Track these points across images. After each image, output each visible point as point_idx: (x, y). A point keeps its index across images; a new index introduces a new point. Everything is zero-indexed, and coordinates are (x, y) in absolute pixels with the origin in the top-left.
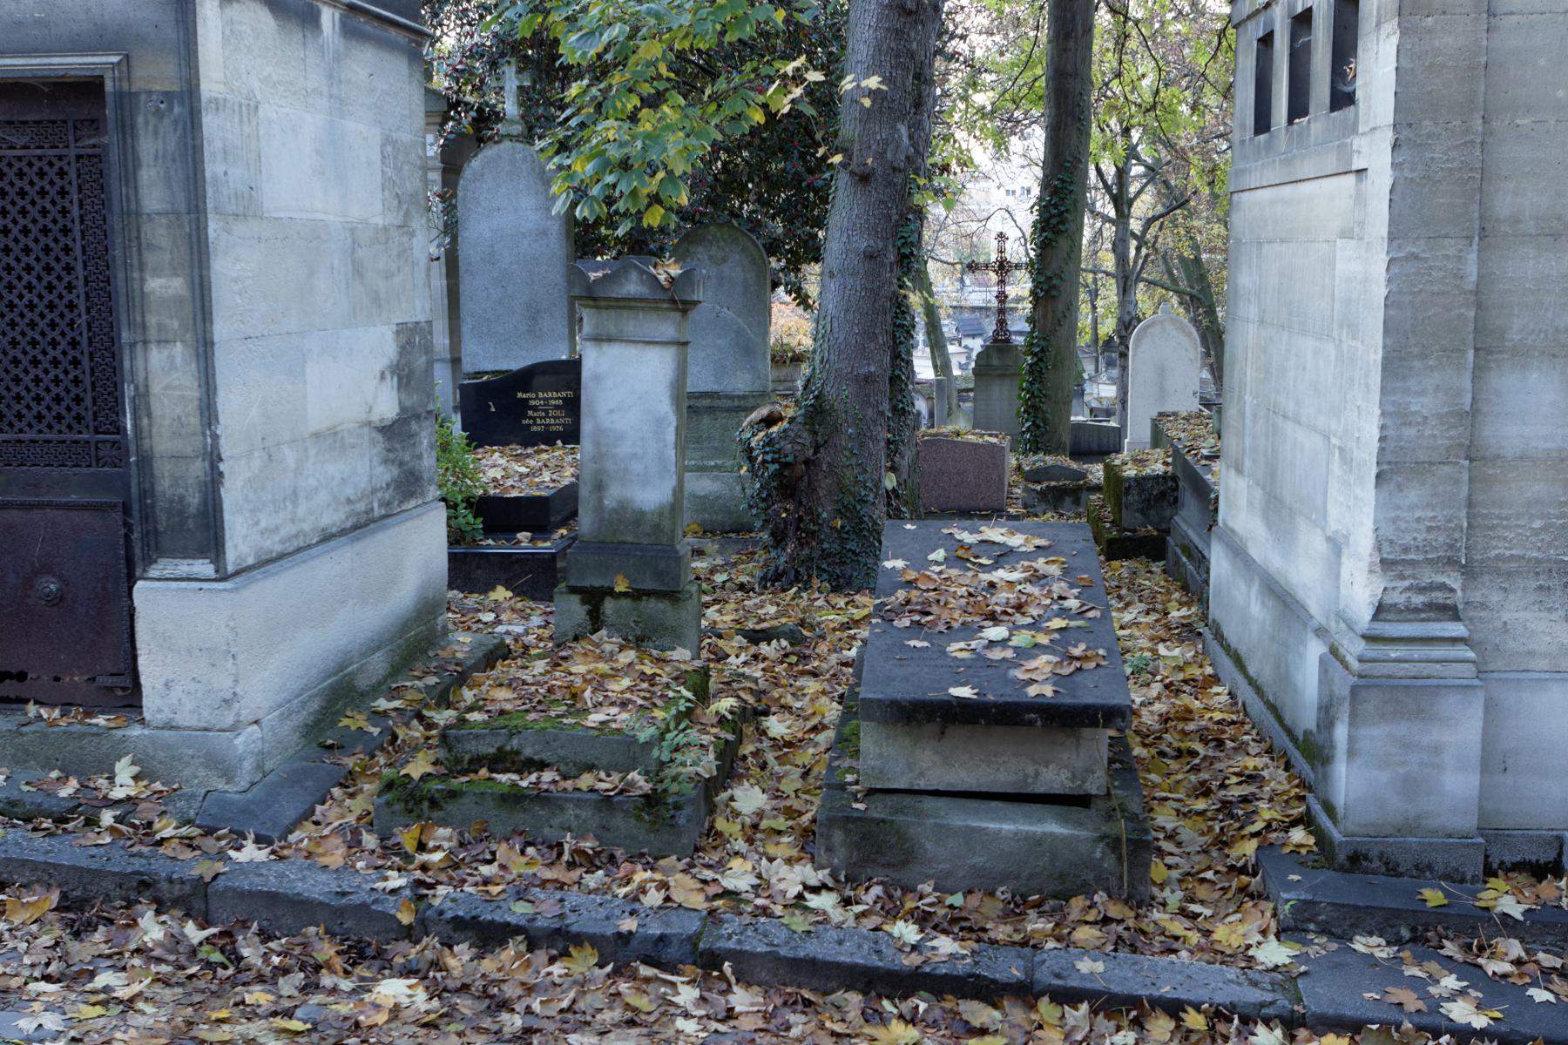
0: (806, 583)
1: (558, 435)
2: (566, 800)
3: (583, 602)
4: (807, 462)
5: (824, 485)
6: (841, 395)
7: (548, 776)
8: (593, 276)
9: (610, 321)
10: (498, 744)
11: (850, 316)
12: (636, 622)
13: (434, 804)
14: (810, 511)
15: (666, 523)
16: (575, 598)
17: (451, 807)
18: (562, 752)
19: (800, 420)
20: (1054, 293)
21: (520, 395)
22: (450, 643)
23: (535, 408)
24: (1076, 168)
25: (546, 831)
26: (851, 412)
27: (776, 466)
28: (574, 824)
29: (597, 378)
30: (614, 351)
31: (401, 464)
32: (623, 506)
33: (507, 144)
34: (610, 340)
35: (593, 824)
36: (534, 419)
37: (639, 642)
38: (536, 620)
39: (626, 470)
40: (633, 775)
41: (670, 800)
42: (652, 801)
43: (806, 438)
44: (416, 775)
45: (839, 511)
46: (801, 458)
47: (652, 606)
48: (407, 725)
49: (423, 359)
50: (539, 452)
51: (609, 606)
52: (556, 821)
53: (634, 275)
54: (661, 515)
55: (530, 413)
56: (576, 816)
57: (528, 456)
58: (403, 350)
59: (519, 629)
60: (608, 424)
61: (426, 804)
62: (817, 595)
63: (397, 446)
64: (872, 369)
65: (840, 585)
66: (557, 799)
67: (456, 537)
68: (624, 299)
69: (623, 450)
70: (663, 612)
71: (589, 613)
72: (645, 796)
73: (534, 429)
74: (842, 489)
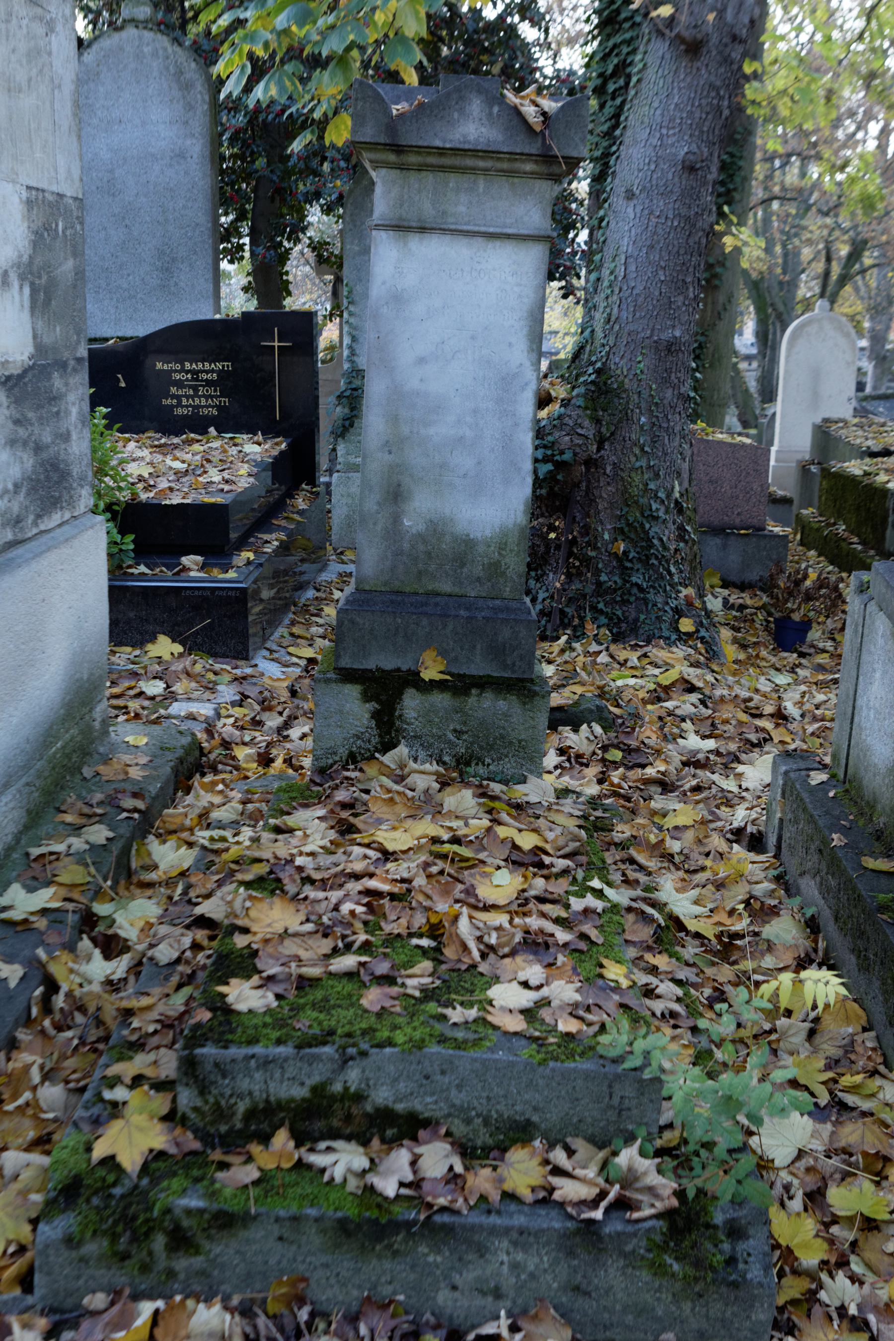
0: (575, 629)
2: (493, 1231)
3: (366, 697)
4: (589, 462)
5: (606, 492)
6: (633, 368)
7: (437, 1159)
8: (396, 109)
9: (424, 194)
10: (316, 1079)
12: (458, 733)
13: (180, 1241)
14: (586, 530)
16: (353, 691)
17: (223, 1249)
18: (458, 1098)
19: (580, 402)
20: (717, 282)
21: (159, 366)
22: (114, 748)
23: (179, 384)
24: (745, 140)
25: (444, 1297)
26: (645, 395)
27: (549, 467)
28: (508, 1282)
29: (398, 299)
30: (430, 249)
31: (38, 448)
32: (436, 529)
33: (131, 32)
34: (423, 229)
35: (551, 1283)
36: (179, 398)
37: (459, 769)
38: (227, 693)
39: (443, 466)
40: (628, 1157)
41: (719, 1218)
42: (685, 1220)
43: (588, 429)
44: (131, 1160)
45: (621, 531)
46: (583, 456)
47: (487, 705)
48: (71, 947)
49: (70, 264)
50: (190, 442)
51: (411, 704)
52: (467, 1277)
53: (476, 106)
54: (502, 547)
55: (173, 390)
56: (515, 1266)
58: (41, 237)
59: (205, 710)
60: (413, 384)
61: (159, 1242)
62: (594, 647)
63: (30, 415)
64: (677, 333)
65: (624, 632)
66: (473, 1228)
67: (116, 569)
68: (456, 151)
69: (441, 430)
70: (506, 715)
71: (376, 715)
72: (668, 1215)
73: (179, 411)
74: (628, 501)
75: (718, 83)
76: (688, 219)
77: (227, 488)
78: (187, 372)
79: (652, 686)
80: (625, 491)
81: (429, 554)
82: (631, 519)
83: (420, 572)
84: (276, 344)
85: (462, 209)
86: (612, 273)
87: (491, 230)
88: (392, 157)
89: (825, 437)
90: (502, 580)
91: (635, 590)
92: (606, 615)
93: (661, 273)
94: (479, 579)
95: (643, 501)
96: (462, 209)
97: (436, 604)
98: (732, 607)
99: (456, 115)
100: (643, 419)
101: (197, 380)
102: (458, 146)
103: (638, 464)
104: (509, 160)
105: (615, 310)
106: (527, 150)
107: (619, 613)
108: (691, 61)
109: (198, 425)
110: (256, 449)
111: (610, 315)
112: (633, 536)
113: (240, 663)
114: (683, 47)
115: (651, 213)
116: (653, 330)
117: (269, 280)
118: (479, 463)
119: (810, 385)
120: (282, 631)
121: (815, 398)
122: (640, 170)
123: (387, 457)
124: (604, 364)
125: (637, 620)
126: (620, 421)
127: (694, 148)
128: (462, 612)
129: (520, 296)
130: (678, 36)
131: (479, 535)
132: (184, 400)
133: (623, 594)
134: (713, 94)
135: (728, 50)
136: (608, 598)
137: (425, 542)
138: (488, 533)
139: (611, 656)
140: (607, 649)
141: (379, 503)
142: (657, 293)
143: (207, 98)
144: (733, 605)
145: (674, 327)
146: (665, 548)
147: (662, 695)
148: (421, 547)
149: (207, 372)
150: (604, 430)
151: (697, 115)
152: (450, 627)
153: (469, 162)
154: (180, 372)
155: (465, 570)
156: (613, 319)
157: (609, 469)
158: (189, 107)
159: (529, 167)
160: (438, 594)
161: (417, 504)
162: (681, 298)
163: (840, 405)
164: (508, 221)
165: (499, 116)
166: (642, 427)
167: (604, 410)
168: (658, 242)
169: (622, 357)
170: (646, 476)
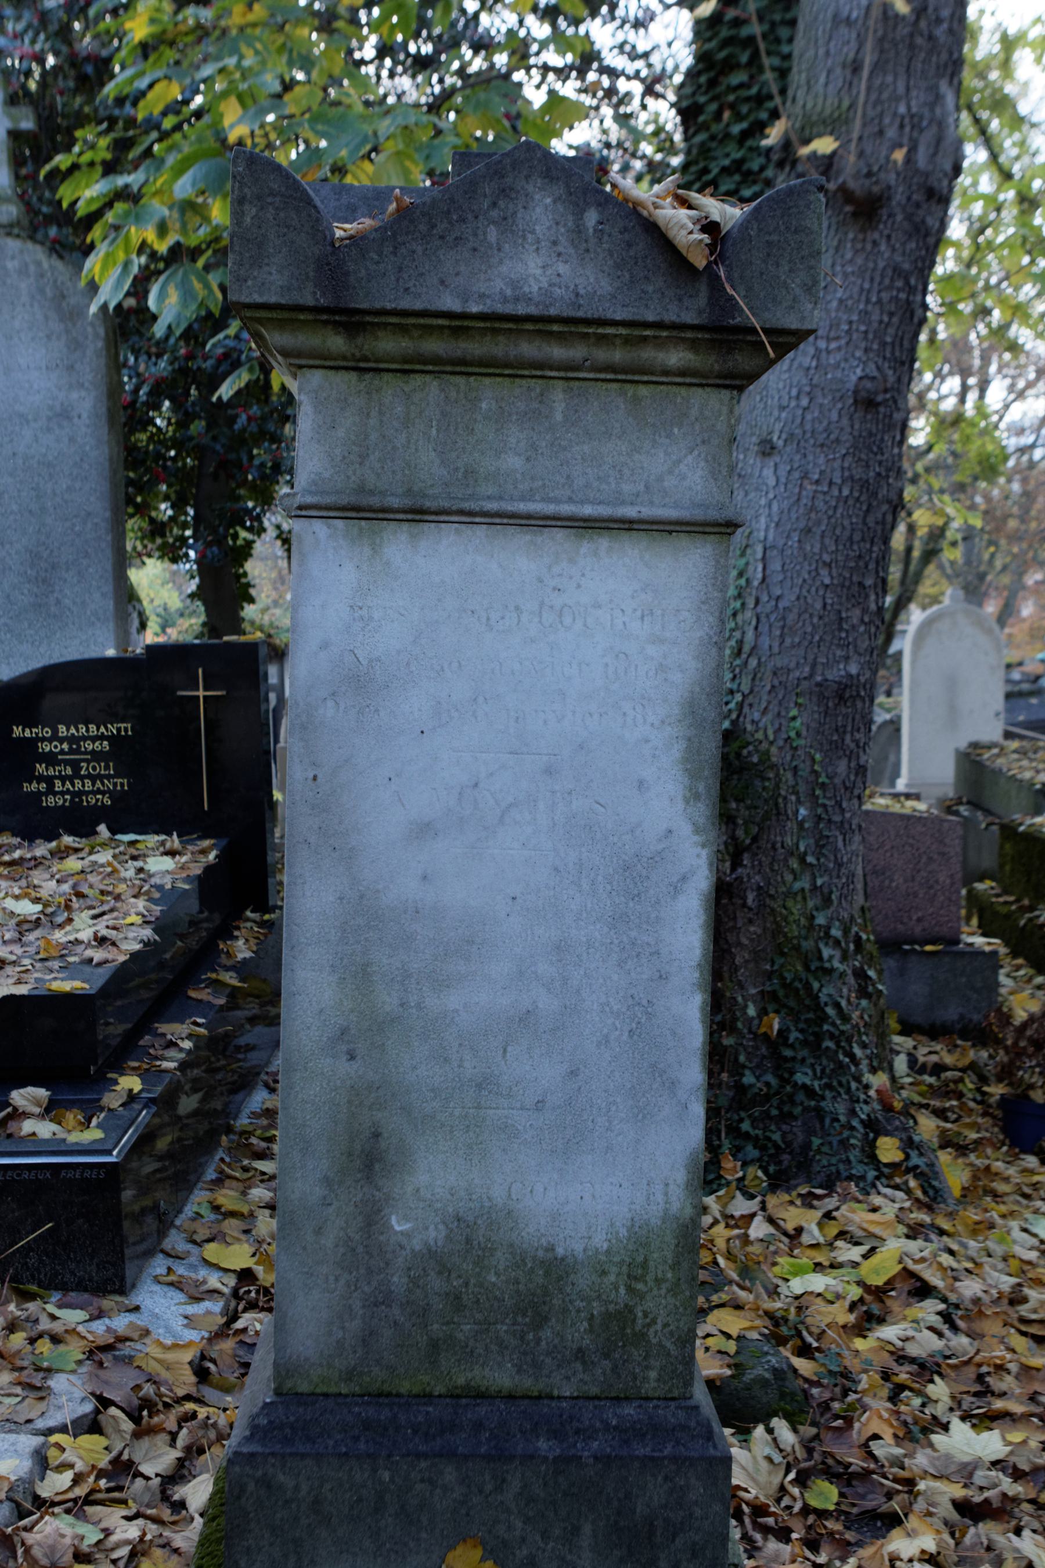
1: (99, 814)
9: (417, 428)
11: (813, 546)
15: (659, 1306)
21: (17, 731)
23: (51, 759)
26: (804, 771)
29: (360, 683)
32: (472, 1237)
34: (418, 514)
36: (50, 781)
39: (484, 1084)
45: (773, 996)
54: (636, 1272)
55: (40, 768)
57: (37, 863)
62: (741, 1206)
64: (853, 669)
68: (495, 322)
75: (906, 266)
76: (865, 484)
77: (98, 955)
78: (61, 741)
79: (855, 1292)
80: (778, 931)
81: (455, 1301)
82: (789, 976)
83: (434, 1345)
84: (201, 693)
85: (513, 462)
86: (741, 575)
87: (588, 510)
88: (336, 342)
89: (973, 764)
90: (637, 1354)
91: (801, 1097)
92: (756, 1142)
93: (824, 572)
94: (580, 1354)
95: (807, 945)
96: (513, 462)
97: (479, 1426)
98: (922, 1070)
99: (492, 234)
100: (803, 811)
101: (77, 751)
102: (500, 308)
103: (797, 886)
104: (627, 341)
105: (750, 635)
106: (671, 316)
107: (776, 1137)
108: (863, 230)
109: (80, 821)
110: (167, 864)
111: (740, 643)
112: (792, 1003)
113: (107, 1303)
114: (848, 208)
115: (805, 476)
116: (814, 666)
117: (223, 588)
118: (573, 1073)
119: (941, 700)
120: (198, 1200)
121: (953, 715)
122: (782, 408)
123: (344, 1067)
124: (734, 723)
125: (807, 1146)
126: (766, 817)
127: (872, 370)
128: (542, 1444)
129: (662, 668)
130: (843, 189)
131: (578, 1247)
132: (58, 783)
133: (782, 1102)
134: (899, 284)
135: (921, 212)
136: (757, 1111)
137: (445, 1271)
138: (600, 1241)
139: (771, 1221)
140: (763, 1208)
141: (327, 1182)
142: (818, 605)
143: (101, 331)
144: (924, 1065)
145: (847, 658)
146: (845, 1018)
147: (876, 1309)
148: (436, 1283)
149: (94, 739)
150: (740, 833)
151: (875, 317)
152: (515, 1485)
153: (528, 349)
154: (50, 740)
155: (547, 1334)
156: (746, 648)
157: (751, 897)
158: (75, 345)
159: (675, 357)
160: (481, 1395)
161: (422, 1178)
162: (857, 612)
163: (985, 722)
164: (627, 488)
165: (599, 233)
166: (801, 824)
167: (738, 800)
168: (819, 523)
169: (765, 712)
170: (811, 904)
